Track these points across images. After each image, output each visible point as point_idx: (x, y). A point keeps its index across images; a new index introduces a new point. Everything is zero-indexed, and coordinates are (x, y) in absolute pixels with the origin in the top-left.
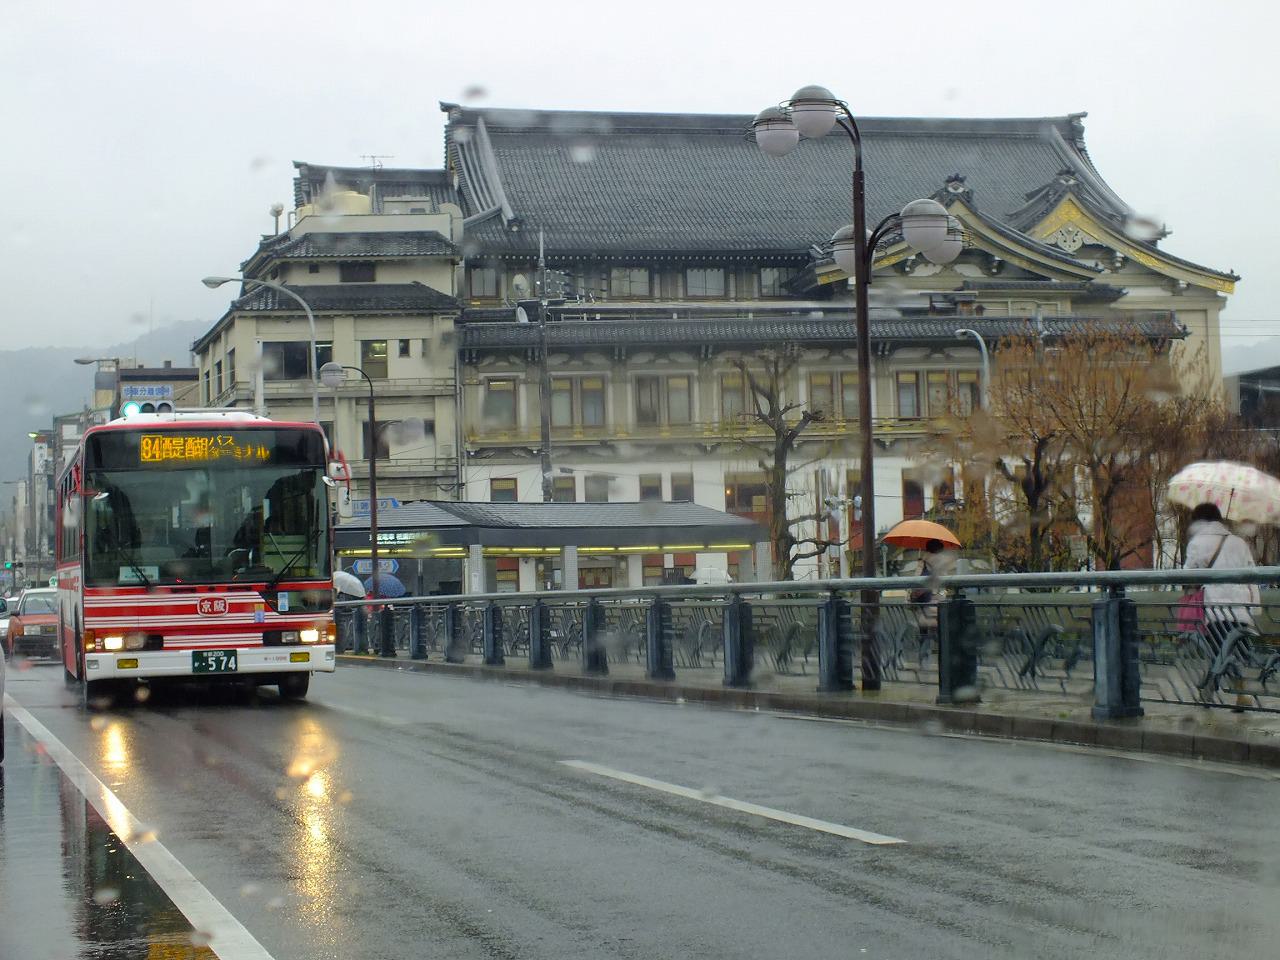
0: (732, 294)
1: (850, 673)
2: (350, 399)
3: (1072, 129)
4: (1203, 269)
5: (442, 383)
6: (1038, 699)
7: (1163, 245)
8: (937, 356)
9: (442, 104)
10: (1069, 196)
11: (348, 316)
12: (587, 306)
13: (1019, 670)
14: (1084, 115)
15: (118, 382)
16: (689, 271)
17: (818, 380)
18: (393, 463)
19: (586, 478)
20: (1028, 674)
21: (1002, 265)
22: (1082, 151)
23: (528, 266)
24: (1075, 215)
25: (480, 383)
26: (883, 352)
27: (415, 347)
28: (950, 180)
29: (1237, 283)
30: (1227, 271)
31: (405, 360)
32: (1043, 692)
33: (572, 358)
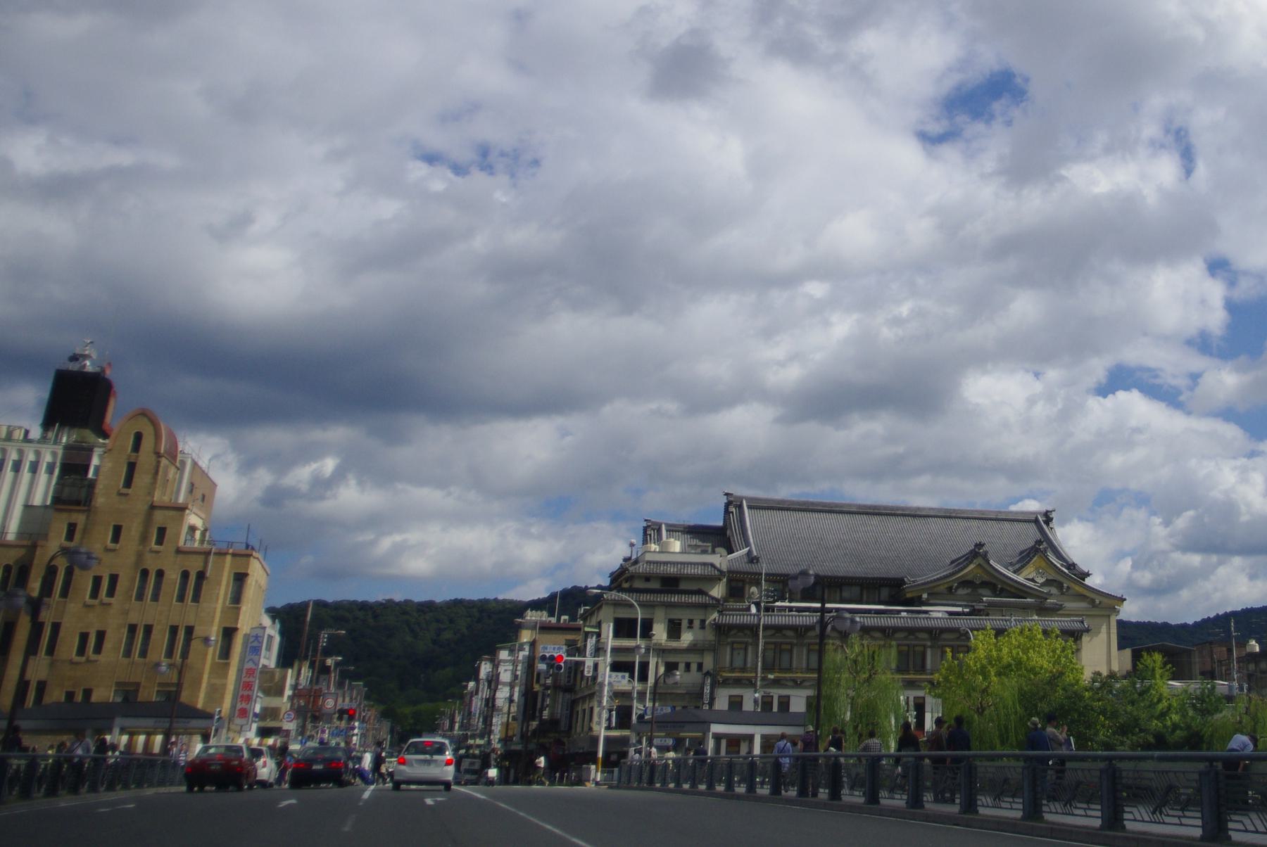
6: (895, 801)
7: (1088, 581)
13: (1152, 809)
19: (914, 698)
20: (1157, 813)
25: (728, 644)
28: (976, 545)
32: (1090, 816)
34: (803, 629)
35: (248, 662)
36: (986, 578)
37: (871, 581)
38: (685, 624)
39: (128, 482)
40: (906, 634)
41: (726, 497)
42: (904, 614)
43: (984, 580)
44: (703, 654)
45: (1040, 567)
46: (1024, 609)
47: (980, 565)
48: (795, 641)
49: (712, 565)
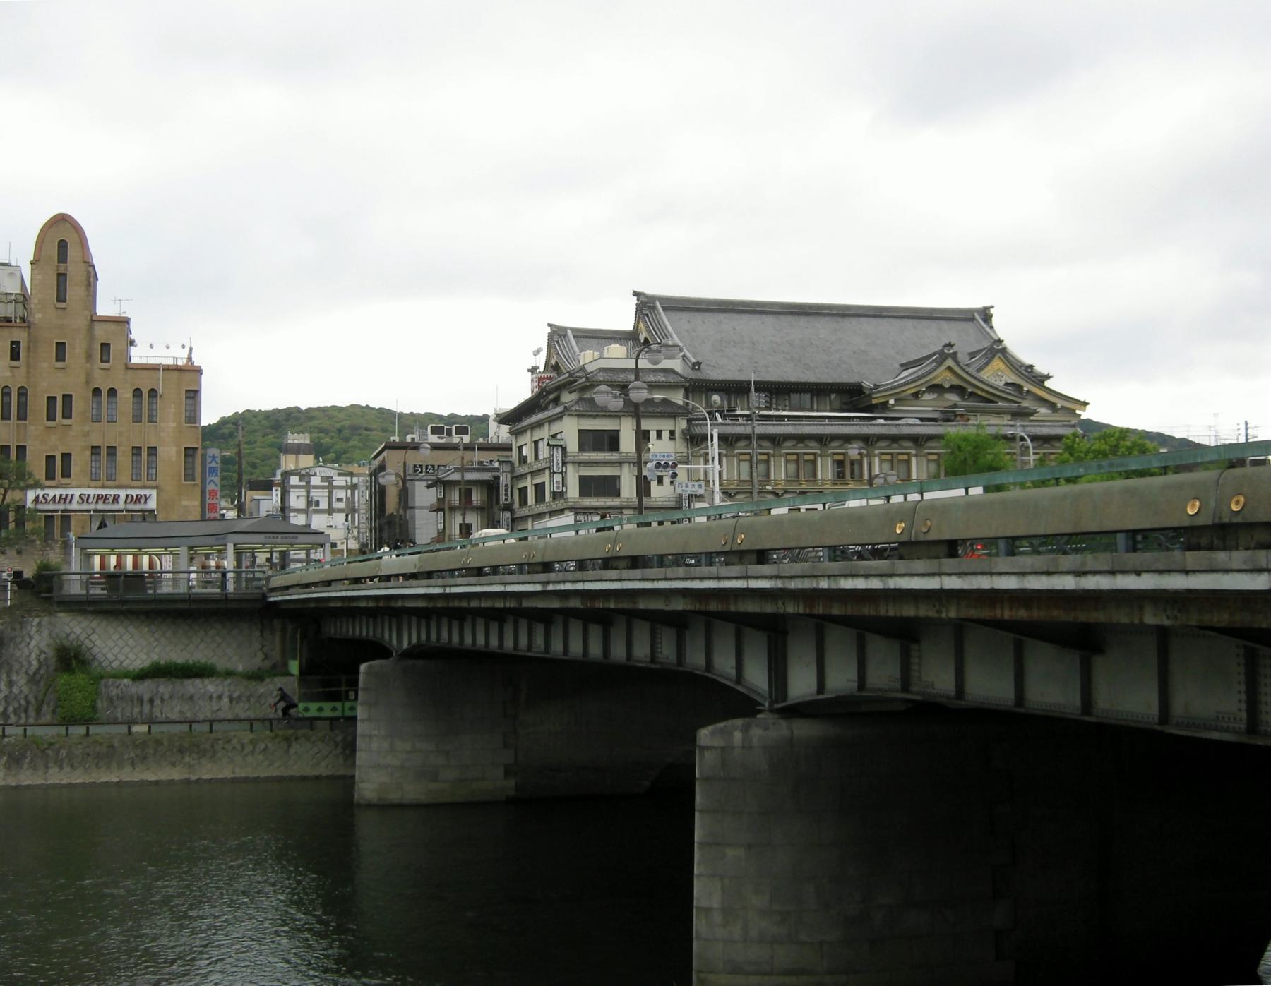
0: (815, 407)
1: (908, 620)
2: (629, 463)
3: (986, 315)
4: (1073, 399)
5: (680, 455)
7: (1047, 384)
8: (800, 445)
9: (634, 292)
10: (999, 355)
11: (629, 416)
12: (777, 413)
14: (992, 307)
15: (620, 453)
16: (791, 394)
17: (884, 457)
18: (654, 499)
21: (972, 394)
22: (992, 327)
23: (704, 389)
24: (1002, 366)
25: (781, 456)
26: (921, 442)
27: (666, 435)
28: (946, 346)
29: (1088, 407)
30: (1082, 400)
31: (659, 442)
33: (1045, 443)
34: (782, 439)
35: (209, 483)
36: (956, 382)
37: (770, 386)
38: (653, 435)
39: (61, 298)
40: (794, 442)
41: (636, 298)
42: (882, 421)
43: (954, 383)
44: (621, 466)
45: (999, 369)
46: (998, 414)
47: (949, 368)
48: (819, 452)
49: (673, 371)
